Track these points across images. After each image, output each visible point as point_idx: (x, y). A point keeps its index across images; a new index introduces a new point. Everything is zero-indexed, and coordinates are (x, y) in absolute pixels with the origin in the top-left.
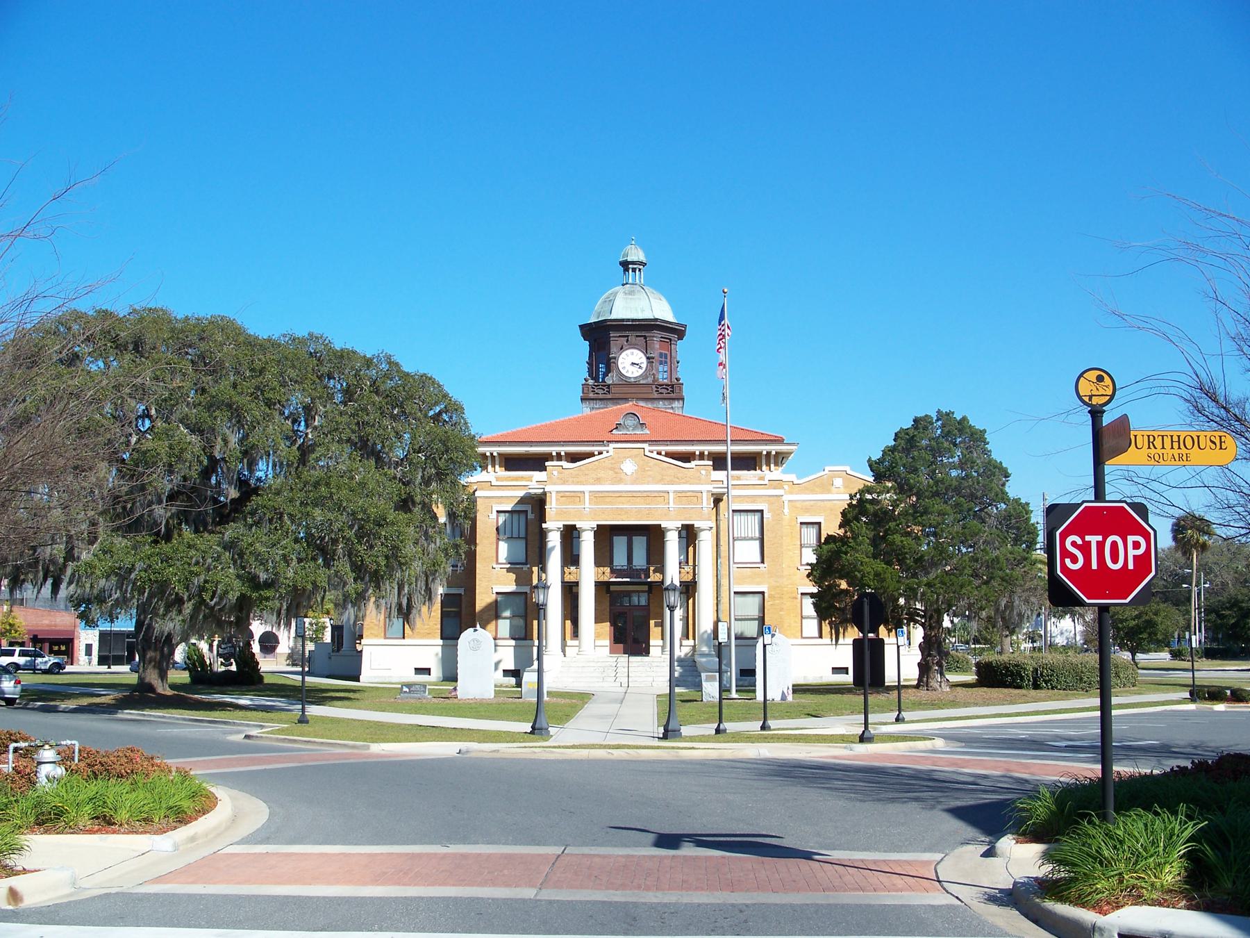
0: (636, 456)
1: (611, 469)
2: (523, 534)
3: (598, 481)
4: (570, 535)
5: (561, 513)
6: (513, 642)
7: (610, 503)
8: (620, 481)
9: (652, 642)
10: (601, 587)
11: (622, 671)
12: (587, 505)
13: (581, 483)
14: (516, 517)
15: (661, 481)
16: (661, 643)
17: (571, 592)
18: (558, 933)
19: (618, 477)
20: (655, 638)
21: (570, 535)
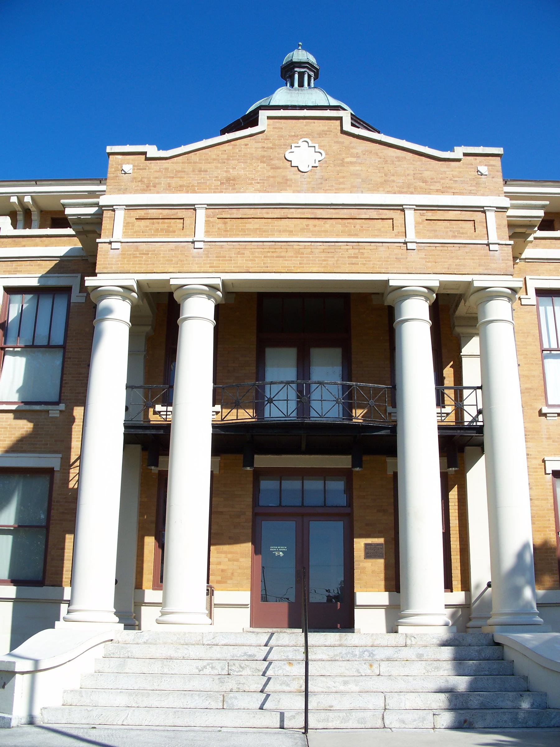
0: (322, 134)
1: (262, 159)
2: (58, 338)
3: (230, 183)
4: (158, 316)
5: (133, 251)
6: (11, 591)
7: (260, 231)
8: (283, 185)
9: (361, 597)
10: (227, 443)
11: (288, 673)
12: (200, 235)
13: (190, 189)
14: (46, 303)
15: (382, 186)
16: (384, 598)
17: (148, 446)
18: (215, 381)
19: (281, 173)
20: (368, 587)
21: (158, 316)
